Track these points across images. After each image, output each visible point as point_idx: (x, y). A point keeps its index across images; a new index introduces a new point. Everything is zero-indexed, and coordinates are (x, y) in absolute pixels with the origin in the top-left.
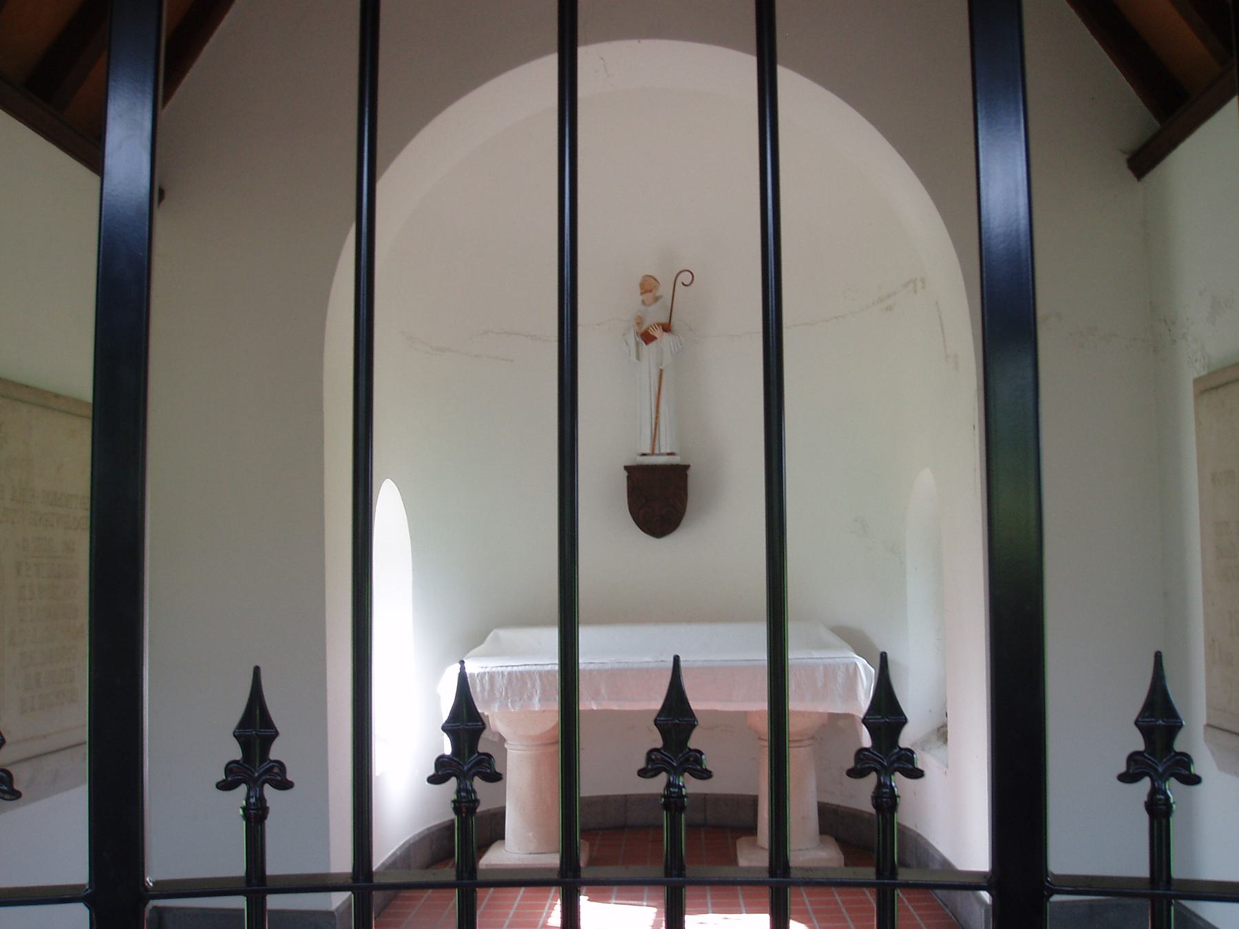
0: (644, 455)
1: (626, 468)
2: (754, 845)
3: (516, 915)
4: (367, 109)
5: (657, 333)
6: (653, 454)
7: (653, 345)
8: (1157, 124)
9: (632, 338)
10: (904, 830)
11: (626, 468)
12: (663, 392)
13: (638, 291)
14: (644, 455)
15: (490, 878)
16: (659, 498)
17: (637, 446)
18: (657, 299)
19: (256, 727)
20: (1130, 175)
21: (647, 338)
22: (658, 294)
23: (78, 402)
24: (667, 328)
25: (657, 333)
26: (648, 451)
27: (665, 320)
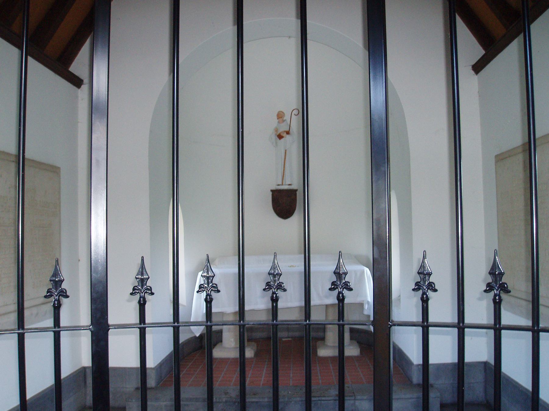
0: (278, 185)
1: (272, 191)
2: (327, 347)
3: (192, 365)
4: (526, 19)
5: (284, 135)
6: (282, 185)
7: (282, 140)
8: (483, 52)
9: (274, 137)
10: (395, 347)
11: (272, 191)
12: (287, 159)
13: (276, 117)
14: (278, 185)
15: (491, 391)
16: (285, 203)
17: (274, 182)
18: (284, 121)
19: (57, 282)
20: (473, 72)
21: (280, 137)
22: (284, 119)
23: (8, 154)
24: (288, 133)
25: (284, 135)
26: (280, 183)
27: (287, 129)
